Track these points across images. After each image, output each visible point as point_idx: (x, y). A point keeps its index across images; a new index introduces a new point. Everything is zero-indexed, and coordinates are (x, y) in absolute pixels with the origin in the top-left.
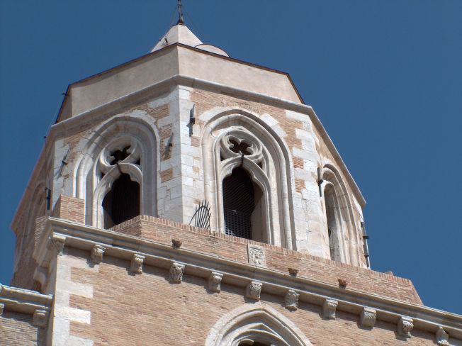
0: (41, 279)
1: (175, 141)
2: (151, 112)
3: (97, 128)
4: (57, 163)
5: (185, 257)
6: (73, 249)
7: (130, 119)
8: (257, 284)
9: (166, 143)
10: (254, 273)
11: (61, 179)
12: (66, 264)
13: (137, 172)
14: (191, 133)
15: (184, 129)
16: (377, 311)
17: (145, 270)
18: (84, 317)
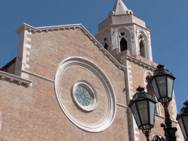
0: (124, 63)
1: (134, 36)
2: (129, 28)
3: (119, 28)
4: (112, 32)
5: (141, 62)
6: (129, 60)
7: (125, 28)
8: (149, 67)
9: (132, 36)
10: (149, 66)
11: (113, 36)
12: (128, 62)
13: (126, 39)
14: (136, 35)
15: (135, 34)
16: (20, 75)
17: (136, 64)
18: (29, 53)
